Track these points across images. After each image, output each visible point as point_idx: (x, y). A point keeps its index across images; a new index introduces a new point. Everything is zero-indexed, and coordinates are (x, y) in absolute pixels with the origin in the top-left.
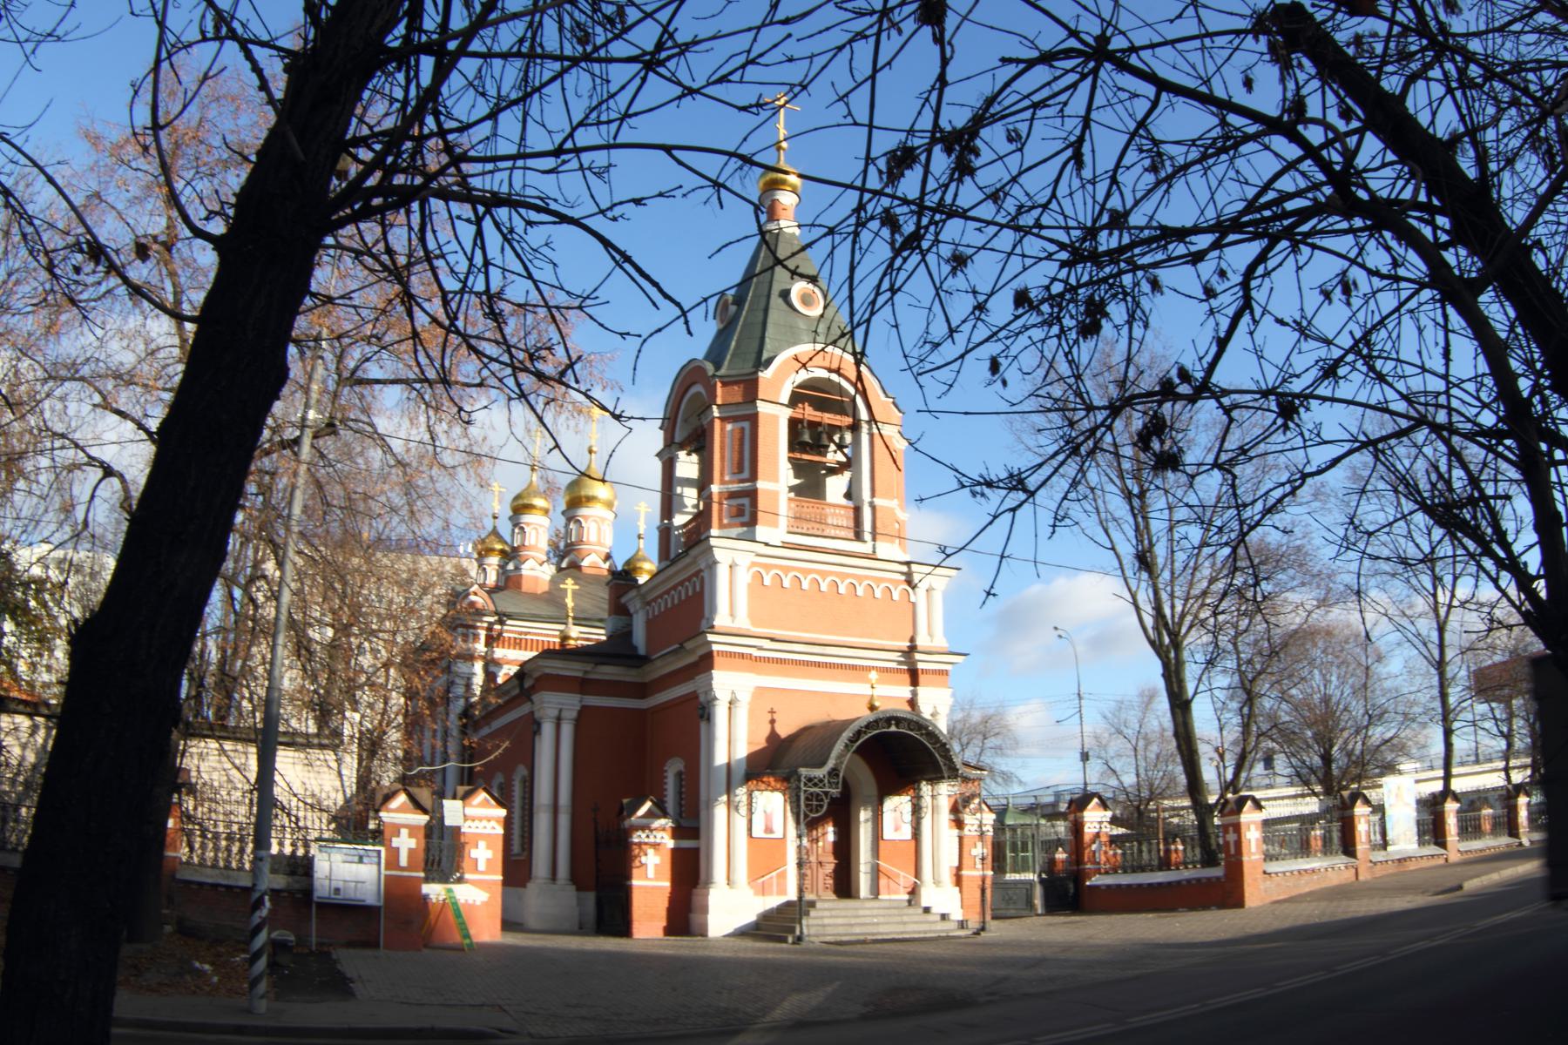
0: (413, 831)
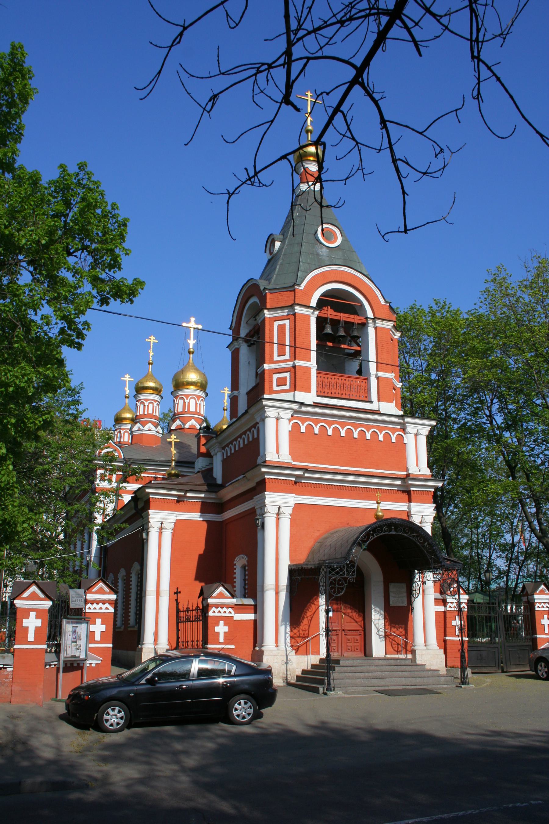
0: (39, 613)
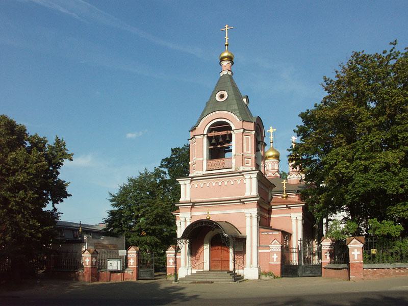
0: (358, 249)
